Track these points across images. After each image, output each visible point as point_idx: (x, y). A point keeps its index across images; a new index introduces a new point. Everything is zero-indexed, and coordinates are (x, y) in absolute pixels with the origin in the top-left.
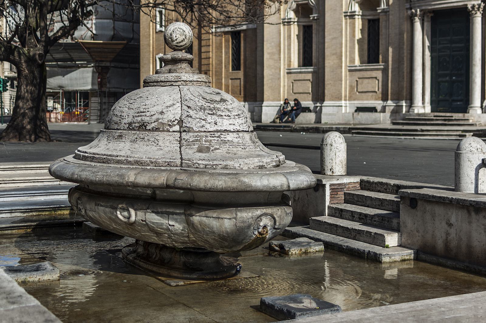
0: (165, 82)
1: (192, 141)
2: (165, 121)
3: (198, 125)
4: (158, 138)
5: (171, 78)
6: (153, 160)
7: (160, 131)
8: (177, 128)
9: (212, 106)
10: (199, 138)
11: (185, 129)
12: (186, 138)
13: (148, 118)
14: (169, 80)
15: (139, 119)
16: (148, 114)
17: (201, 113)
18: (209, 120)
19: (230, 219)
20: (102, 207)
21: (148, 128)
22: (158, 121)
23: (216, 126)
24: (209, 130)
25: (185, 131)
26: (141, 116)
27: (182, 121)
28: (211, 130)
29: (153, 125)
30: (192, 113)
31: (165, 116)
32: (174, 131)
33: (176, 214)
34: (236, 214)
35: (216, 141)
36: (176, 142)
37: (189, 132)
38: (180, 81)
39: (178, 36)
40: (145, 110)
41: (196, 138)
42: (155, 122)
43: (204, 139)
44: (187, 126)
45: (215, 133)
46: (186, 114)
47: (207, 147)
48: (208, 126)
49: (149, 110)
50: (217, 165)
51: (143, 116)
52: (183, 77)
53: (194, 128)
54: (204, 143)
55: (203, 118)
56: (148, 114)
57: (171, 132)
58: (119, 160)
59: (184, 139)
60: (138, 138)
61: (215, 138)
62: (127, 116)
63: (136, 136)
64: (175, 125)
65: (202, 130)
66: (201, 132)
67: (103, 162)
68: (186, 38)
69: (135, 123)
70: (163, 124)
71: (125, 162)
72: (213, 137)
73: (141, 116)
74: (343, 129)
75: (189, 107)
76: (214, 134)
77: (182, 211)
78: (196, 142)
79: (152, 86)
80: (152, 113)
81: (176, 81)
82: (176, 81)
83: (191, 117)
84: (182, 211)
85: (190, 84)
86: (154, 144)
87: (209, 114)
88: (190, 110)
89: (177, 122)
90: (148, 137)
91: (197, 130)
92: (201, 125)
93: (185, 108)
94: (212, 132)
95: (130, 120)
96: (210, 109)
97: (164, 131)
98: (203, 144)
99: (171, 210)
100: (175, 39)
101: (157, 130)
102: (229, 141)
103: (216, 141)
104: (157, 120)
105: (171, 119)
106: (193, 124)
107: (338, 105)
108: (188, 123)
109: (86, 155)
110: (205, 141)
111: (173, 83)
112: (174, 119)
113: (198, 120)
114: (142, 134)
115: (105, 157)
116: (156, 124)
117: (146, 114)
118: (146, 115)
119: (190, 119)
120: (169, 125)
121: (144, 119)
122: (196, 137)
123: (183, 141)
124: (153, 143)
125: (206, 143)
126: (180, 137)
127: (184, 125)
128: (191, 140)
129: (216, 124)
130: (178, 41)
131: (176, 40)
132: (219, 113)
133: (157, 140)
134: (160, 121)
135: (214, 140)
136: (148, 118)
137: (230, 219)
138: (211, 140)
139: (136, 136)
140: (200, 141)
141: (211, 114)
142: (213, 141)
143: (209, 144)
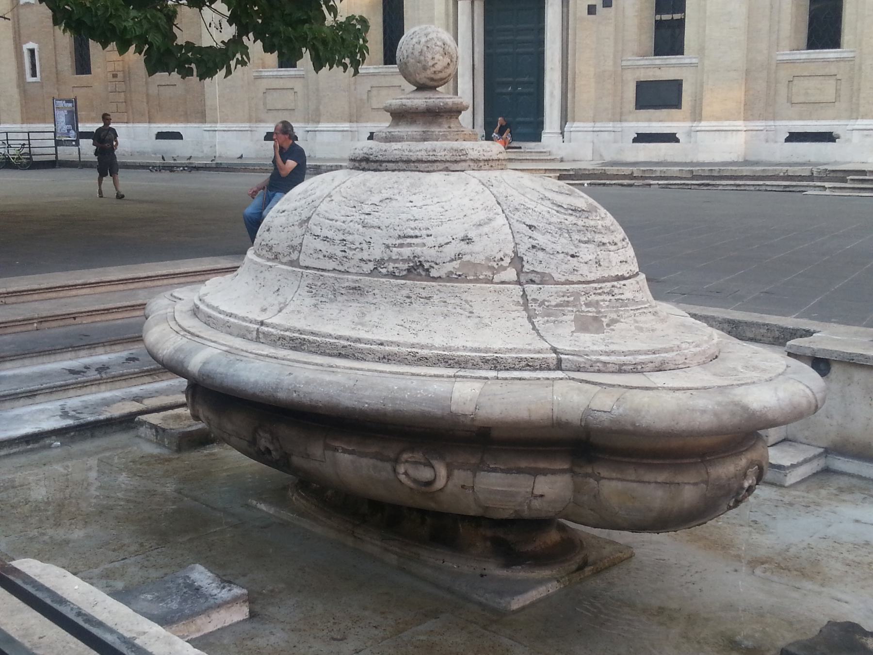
0: (429, 161)
1: (557, 306)
2: (480, 259)
3: (564, 267)
4: (469, 299)
5: (443, 153)
6: (489, 355)
7: (470, 281)
8: (511, 274)
9: (580, 223)
10: (572, 299)
11: (532, 276)
12: (541, 297)
13: (433, 252)
14: (439, 158)
15: (406, 252)
16: (430, 241)
17: (563, 240)
18: (584, 256)
19: (695, 484)
20: (346, 456)
21: (434, 273)
22: (460, 258)
23: (599, 268)
24: (589, 279)
25: (532, 282)
26: (410, 245)
27: (522, 259)
28: (593, 279)
29: (449, 267)
30: (541, 239)
31: (476, 247)
32: (503, 283)
33: (554, 472)
34: (707, 473)
35: (607, 303)
36: (515, 308)
37: (542, 282)
38: (465, 161)
39: (437, 57)
40: (417, 233)
41: (566, 299)
42: (452, 260)
43: (583, 299)
44: (538, 270)
45: (603, 285)
46: (528, 243)
47: (596, 319)
48: (584, 269)
49: (429, 232)
50: (643, 363)
51: (417, 245)
52: (471, 152)
53: (556, 276)
54: (584, 308)
55: (571, 253)
56: (430, 241)
57: (497, 283)
58: (451, 366)
59: (535, 300)
60: (414, 296)
61: (604, 297)
62: (365, 246)
63: (405, 292)
64: (505, 269)
65: (574, 278)
66: (572, 283)
67: (340, 355)
68: (451, 61)
69: (396, 261)
70: (475, 265)
71: (408, 357)
72: (600, 294)
73: (410, 245)
74: (325, 168)
75: (530, 227)
76: (601, 288)
77: (566, 466)
78: (568, 306)
79: (393, 171)
80: (442, 240)
81: (456, 162)
82: (456, 162)
83: (543, 250)
84: (566, 466)
85: (487, 167)
86: (461, 311)
87: (580, 241)
88: (535, 234)
89: (507, 260)
90: (441, 295)
91: (563, 279)
92: (570, 267)
93: (519, 227)
94: (593, 282)
95: (377, 252)
96: (579, 231)
97: (477, 280)
98: (583, 311)
99: (542, 465)
100: (430, 64)
101: (450, 278)
102: (629, 300)
103: (607, 303)
104: (459, 256)
105: (494, 254)
106: (552, 266)
107: (342, 129)
108: (532, 262)
109: (232, 320)
110: (587, 305)
111: (447, 165)
112: (501, 255)
113: (561, 256)
114: (419, 286)
115: (346, 343)
116: (456, 264)
117: (424, 241)
118: (424, 245)
119: (541, 255)
120: (491, 268)
121: (420, 254)
122: (563, 296)
123: (532, 306)
124: (458, 310)
125: (590, 309)
126: (524, 295)
127: (527, 267)
128: (554, 303)
129: (600, 265)
130: (438, 67)
131: (433, 66)
132: (598, 238)
133: (466, 301)
134: (466, 258)
135: (604, 300)
136: (433, 252)
137: (695, 484)
138: (597, 302)
139: (405, 292)
140: (575, 306)
141: (586, 242)
142: (602, 303)
143: (594, 309)
